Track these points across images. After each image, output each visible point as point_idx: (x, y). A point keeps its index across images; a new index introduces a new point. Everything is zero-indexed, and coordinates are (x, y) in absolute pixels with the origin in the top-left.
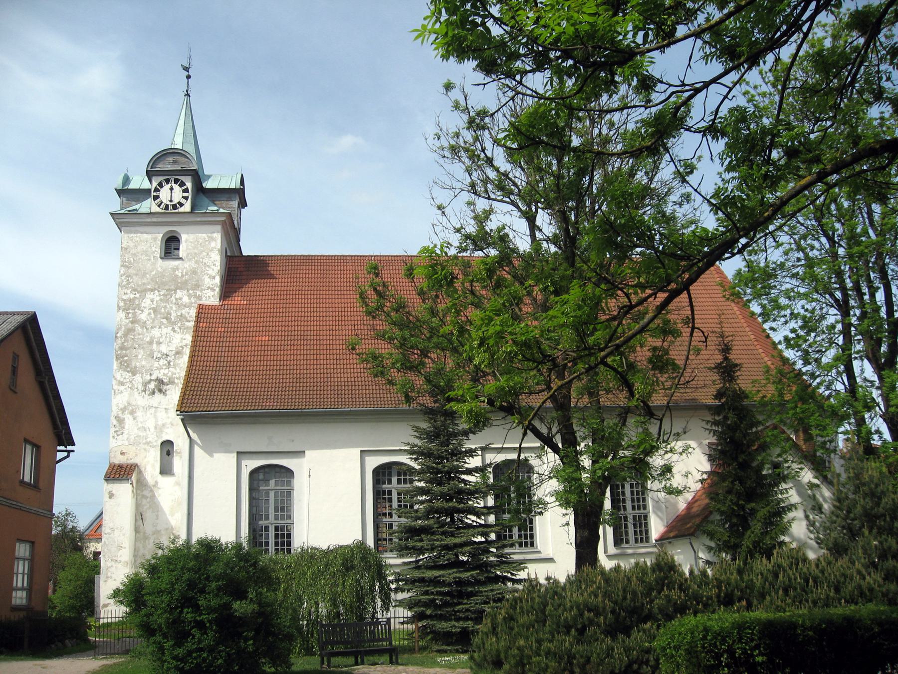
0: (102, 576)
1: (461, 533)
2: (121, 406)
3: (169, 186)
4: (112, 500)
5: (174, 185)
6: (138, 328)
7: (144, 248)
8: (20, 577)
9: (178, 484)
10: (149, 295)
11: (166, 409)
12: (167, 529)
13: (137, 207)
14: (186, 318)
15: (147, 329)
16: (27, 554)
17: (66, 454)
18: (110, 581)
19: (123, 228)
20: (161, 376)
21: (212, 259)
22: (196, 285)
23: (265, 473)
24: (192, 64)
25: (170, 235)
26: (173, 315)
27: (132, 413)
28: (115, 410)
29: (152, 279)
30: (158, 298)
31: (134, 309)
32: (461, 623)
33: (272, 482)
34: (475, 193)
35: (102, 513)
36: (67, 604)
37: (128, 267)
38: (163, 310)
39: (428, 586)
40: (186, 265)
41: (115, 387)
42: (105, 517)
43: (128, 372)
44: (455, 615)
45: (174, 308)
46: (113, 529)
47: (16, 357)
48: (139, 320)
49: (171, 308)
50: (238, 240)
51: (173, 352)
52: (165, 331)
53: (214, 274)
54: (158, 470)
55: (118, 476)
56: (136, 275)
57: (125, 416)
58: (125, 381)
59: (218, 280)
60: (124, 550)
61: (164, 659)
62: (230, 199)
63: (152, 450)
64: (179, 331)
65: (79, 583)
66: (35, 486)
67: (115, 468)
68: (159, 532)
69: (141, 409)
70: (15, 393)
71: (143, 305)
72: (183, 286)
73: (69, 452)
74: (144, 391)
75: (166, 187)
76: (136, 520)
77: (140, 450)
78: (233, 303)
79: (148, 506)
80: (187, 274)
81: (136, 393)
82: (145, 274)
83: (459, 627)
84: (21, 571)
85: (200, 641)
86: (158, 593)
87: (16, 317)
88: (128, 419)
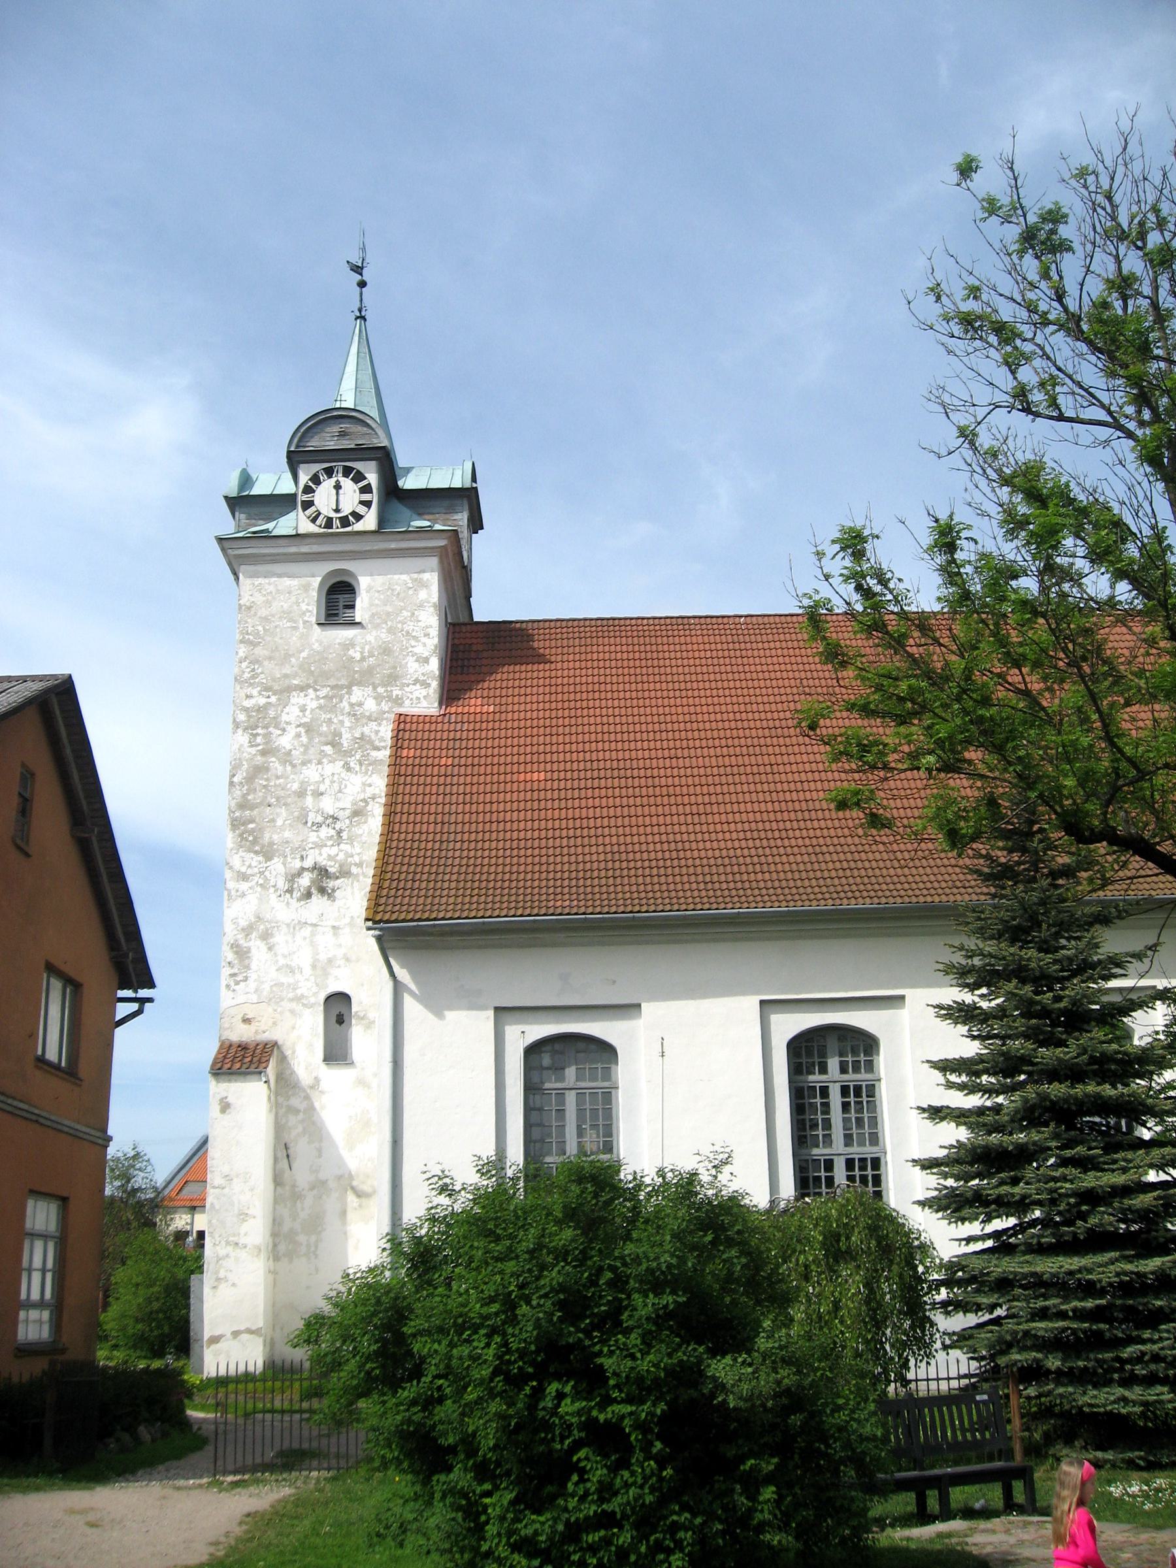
0: (208, 1277)
1: (1115, 1162)
2: (243, 923)
4: (226, 1116)
5: (342, 480)
6: (276, 765)
7: (286, 606)
8: (36, 1277)
9: (361, 1082)
10: (297, 699)
11: (334, 927)
12: (339, 1178)
13: (270, 526)
14: (371, 742)
15: (294, 766)
16: (53, 1227)
17: (135, 1007)
18: (222, 1286)
19: (243, 570)
20: (323, 861)
21: (421, 624)
22: (390, 676)
23: (554, 1053)
24: (367, 260)
25: (338, 579)
26: (346, 740)
27: (266, 936)
28: (231, 932)
29: (301, 666)
30: (314, 704)
31: (266, 727)
32: (1138, 1390)
33: (571, 1072)
34: (1027, 410)
35: (205, 1141)
36: (131, 1331)
37: (254, 644)
38: (324, 728)
39: (1045, 1297)
40: (370, 638)
41: (231, 885)
42: (215, 1153)
43: (256, 853)
44: (1121, 1370)
45: (347, 724)
46: (228, 1178)
47: (28, 776)
48: (277, 749)
49: (342, 722)
50: (468, 595)
51: (348, 813)
52: (329, 769)
53: (426, 654)
54: (320, 1054)
55: (238, 1065)
56: (270, 658)
57: (251, 944)
58: (249, 872)
59: (434, 665)
61: (485, 1547)
62: (451, 510)
63: (307, 1012)
64: (357, 768)
65: (156, 1289)
66: (70, 1072)
67: (233, 1051)
68: (324, 1183)
69: (284, 929)
70: (27, 855)
71: (284, 717)
72: (363, 678)
73: (143, 1001)
74: (290, 891)
75: (328, 484)
76: (276, 1160)
77: (281, 1013)
78: (466, 709)
79: (300, 1129)
80: (371, 655)
81: (273, 897)
82: (287, 656)
83: (1134, 1403)
84: (37, 1262)
85: (606, 1491)
86: (460, 1330)
87: (29, 684)
88: (258, 950)
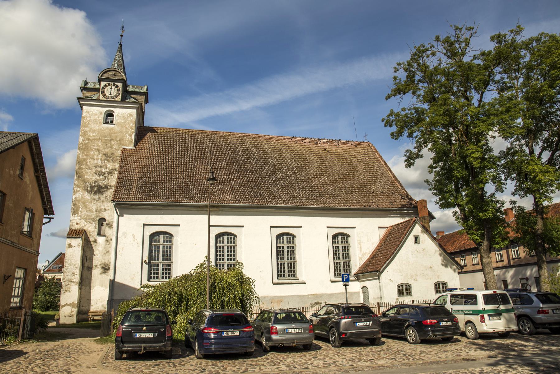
3: (110, 86)
8: (17, 289)
17: (48, 220)
60: (76, 276)
74: (91, 191)
75: (109, 87)
84: (17, 286)
